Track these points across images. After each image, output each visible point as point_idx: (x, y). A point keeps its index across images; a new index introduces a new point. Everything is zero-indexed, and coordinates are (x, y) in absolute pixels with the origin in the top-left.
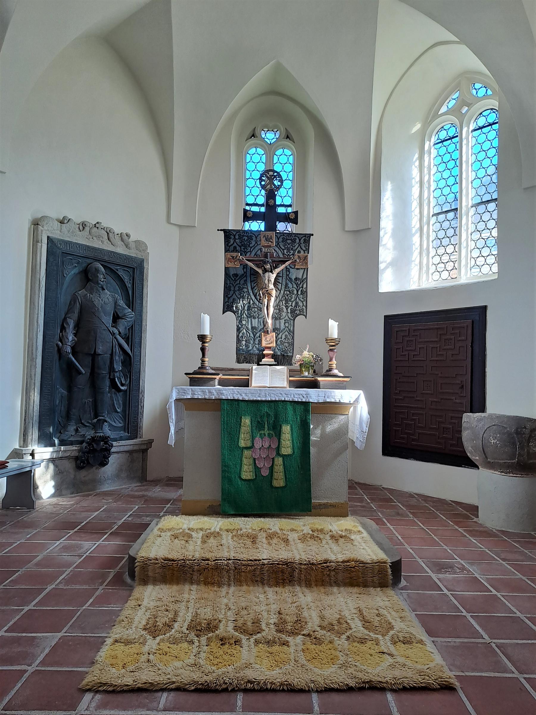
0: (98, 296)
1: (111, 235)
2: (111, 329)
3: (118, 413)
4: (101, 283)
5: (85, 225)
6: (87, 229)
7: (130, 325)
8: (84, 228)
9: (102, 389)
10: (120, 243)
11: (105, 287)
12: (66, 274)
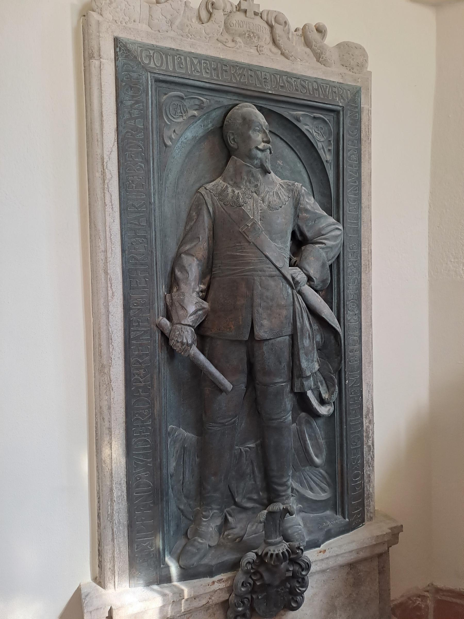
0: (253, 189)
1: (279, 29)
2: (289, 272)
3: (316, 466)
4: (260, 154)
5: (213, 4)
6: (219, 15)
7: (333, 258)
8: (211, 14)
9: (276, 419)
10: (301, 49)
11: (268, 166)
12: (171, 139)
